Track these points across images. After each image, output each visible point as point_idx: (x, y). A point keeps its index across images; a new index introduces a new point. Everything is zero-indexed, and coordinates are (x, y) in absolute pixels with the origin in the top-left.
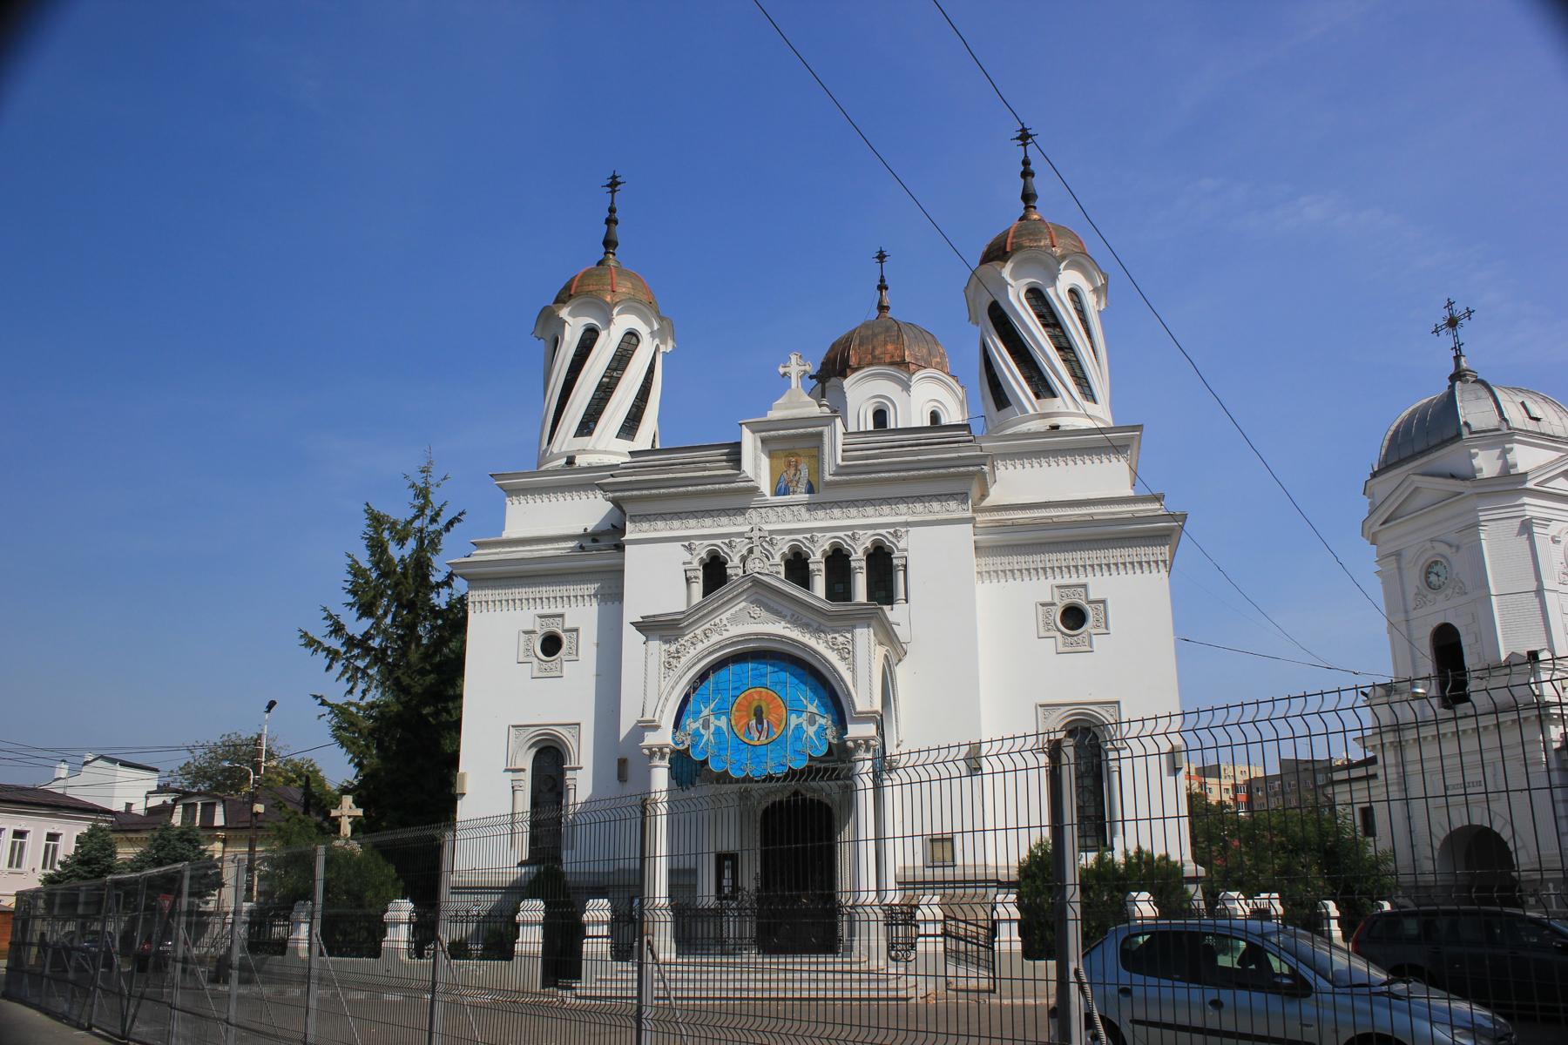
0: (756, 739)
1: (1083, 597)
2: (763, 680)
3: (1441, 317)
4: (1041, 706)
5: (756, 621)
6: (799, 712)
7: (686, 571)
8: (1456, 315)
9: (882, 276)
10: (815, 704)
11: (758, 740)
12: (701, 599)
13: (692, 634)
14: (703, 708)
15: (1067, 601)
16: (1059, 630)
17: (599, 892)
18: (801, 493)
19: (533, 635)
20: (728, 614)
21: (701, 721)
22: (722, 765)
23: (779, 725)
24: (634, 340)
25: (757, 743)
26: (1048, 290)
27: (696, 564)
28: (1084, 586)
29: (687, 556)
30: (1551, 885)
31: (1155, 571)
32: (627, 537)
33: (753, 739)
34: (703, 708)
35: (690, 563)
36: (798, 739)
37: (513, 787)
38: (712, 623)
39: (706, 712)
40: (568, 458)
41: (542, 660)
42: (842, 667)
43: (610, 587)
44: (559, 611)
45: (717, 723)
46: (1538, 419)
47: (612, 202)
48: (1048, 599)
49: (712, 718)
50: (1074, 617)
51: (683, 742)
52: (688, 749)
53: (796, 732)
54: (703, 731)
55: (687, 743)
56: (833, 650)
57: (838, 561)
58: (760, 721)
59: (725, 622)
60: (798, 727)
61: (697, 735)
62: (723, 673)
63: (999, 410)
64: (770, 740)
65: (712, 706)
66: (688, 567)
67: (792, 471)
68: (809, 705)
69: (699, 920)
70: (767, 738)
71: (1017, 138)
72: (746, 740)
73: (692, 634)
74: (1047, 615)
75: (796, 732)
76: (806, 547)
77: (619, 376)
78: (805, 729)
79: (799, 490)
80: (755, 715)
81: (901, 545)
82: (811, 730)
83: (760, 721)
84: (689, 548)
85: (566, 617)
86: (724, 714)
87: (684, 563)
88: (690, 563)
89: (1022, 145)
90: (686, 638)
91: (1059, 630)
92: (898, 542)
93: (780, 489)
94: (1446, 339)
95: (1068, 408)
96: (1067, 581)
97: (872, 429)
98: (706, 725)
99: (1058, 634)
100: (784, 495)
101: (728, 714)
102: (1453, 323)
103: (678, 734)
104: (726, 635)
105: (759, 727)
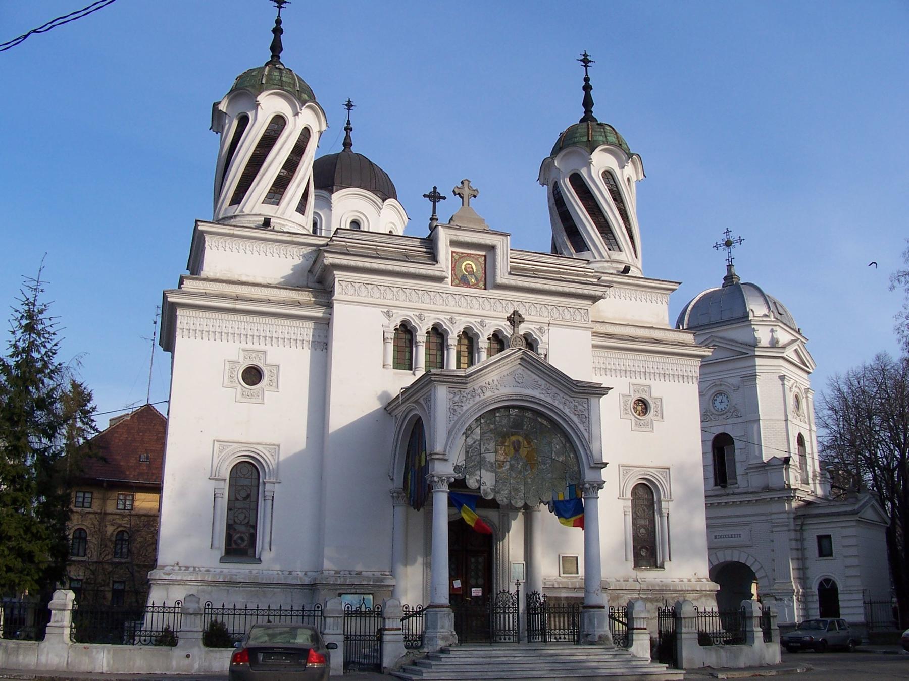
1: (262, 361)
3: (721, 238)
4: (217, 441)
5: (519, 385)
8: (731, 239)
9: (349, 121)
24: (281, 121)
26: (582, 171)
28: (265, 352)
29: (385, 321)
30: (105, 485)
31: (300, 347)
37: (215, 495)
42: (581, 426)
43: (319, 336)
44: (262, 347)
46: (781, 314)
48: (235, 358)
50: (253, 375)
56: (575, 414)
57: (438, 333)
63: (296, 211)
69: (557, 615)
71: (581, 60)
76: (477, 328)
84: (388, 315)
85: (268, 353)
88: (388, 327)
89: (278, 7)
94: (723, 253)
95: (595, 258)
96: (250, 346)
97: (348, 227)
99: (633, 418)
102: (728, 244)
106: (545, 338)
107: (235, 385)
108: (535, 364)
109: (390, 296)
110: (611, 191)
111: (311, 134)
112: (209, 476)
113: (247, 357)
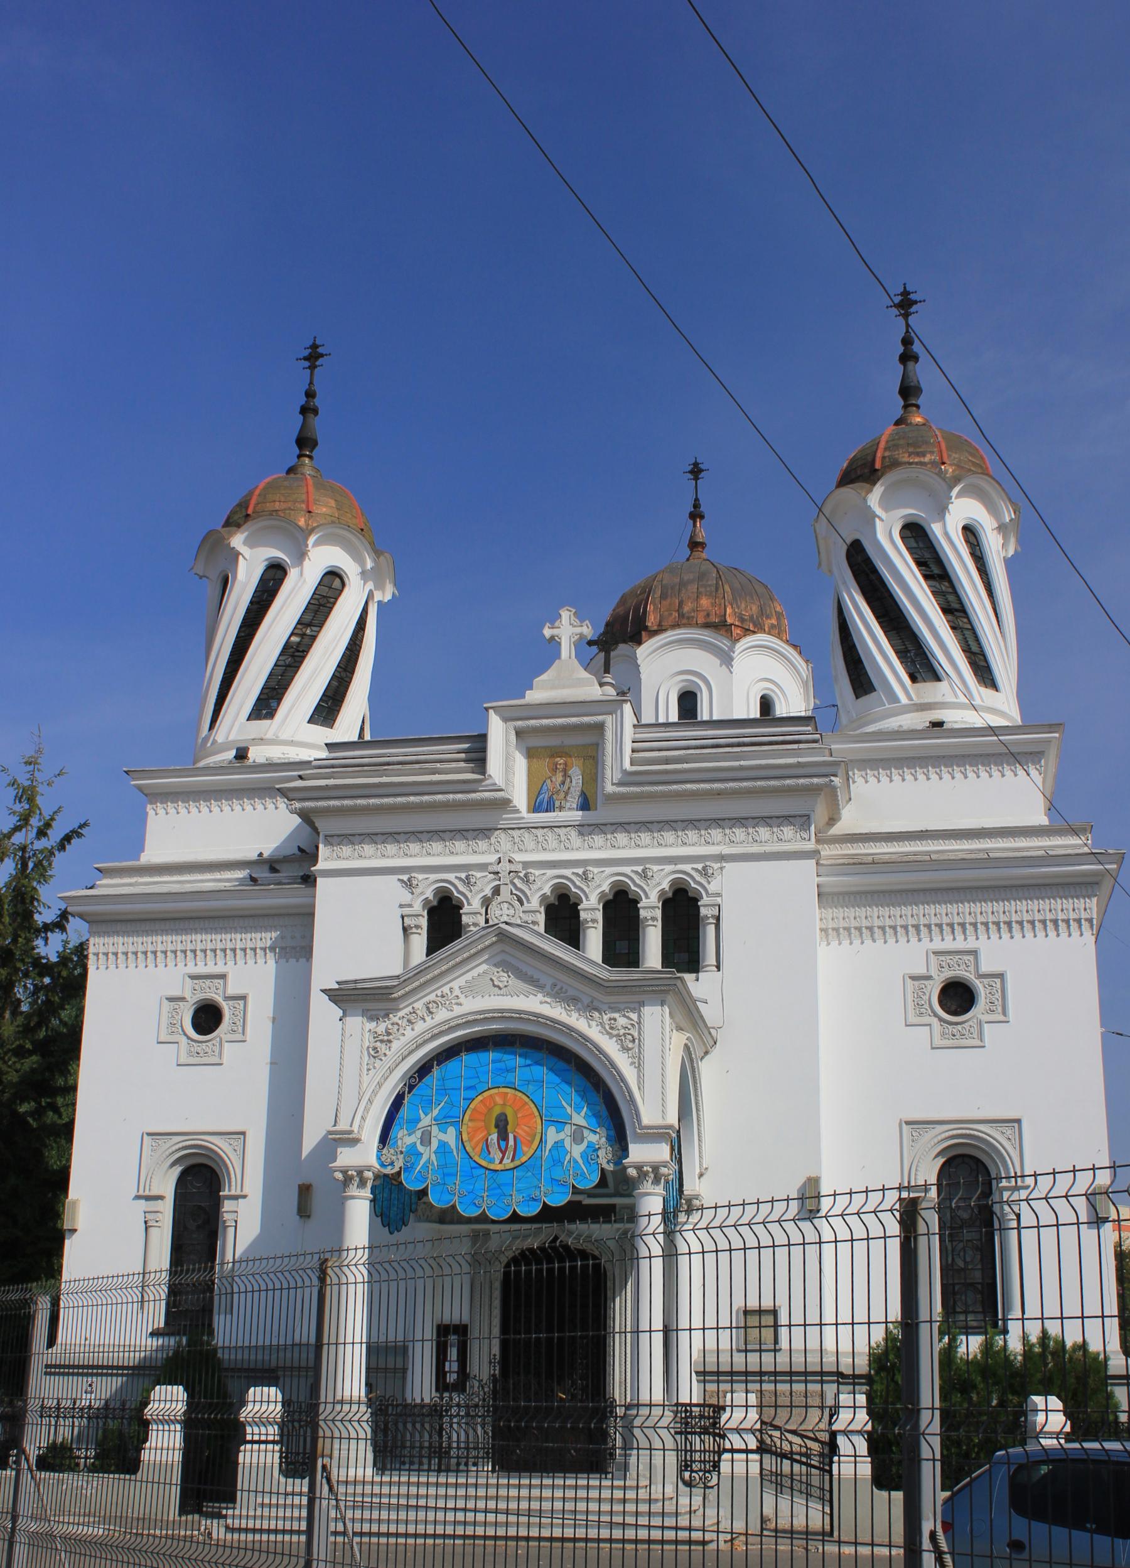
0: (497, 1161)
1: (972, 968)
2: (510, 1077)
5: (499, 992)
6: (560, 1124)
7: (403, 917)
10: (583, 1114)
11: (501, 1162)
12: (424, 958)
13: (410, 1009)
14: (422, 1115)
15: (948, 974)
16: (936, 1015)
17: (266, 1376)
18: (570, 809)
19: (181, 1003)
20: (461, 981)
21: (419, 1134)
22: (446, 1197)
23: (531, 1142)
25: (499, 1167)
27: (418, 907)
28: (974, 953)
32: (321, 865)
33: (492, 1161)
34: (422, 1115)
35: (410, 906)
36: (557, 1162)
37: (146, 1222)
38: (439, 993)
39: (426, 1121)
40: (238, 749)
41: (193, 1040)
43: (293, 938)
44: (219, 969)
45: (442, 1136)
47: (311, 383)
49: (435, 1130)
51: (392, 1164)
52: (399, 1173)
53: (555, 1153)
54: (421, 1148)
55: (399, 1164)
56: (611, 1036)
58: (503, 1136)
59: (457, 992)
60: (559, 1145)
61: (412, 1153)
62: (452, 1065)
64: (517, 1163)
65: (436, 1112)
66: (406, 911)
67: (559, 777)
68: (574, 1115)
70: (513, 1160)
71: (916, 302)
72: (484, 1163)
73: (410, 1009)
74: (919, 994)
75: (555, 1153)
77: (282, 658)
78: (568, 1147)
79: (568, 805)
80: (497, 1126)
81: (712, 887)
82: (577, 1151)
83: (503, 1136)
84: (409, 885)
86: (452, 1124)
87: (401, 906)
88: (410, 906)
90: (401, 1014)
91: (936, 1015)
92: (709, 883)
93: (541, 803)
96: (948, 944)
98: (426, 1139)
100: (547, 811)
101: (458, 1124)
103: (385, 1151)
104: (458, 1011)
105: (503, 1144)
106: (712, 887)
107: (926, 1019)
108: (455, 949)
109: (553, 843)
110: (973, 554)
111: (346, 580)
112: (134, 1193)
113: (944, 964)
